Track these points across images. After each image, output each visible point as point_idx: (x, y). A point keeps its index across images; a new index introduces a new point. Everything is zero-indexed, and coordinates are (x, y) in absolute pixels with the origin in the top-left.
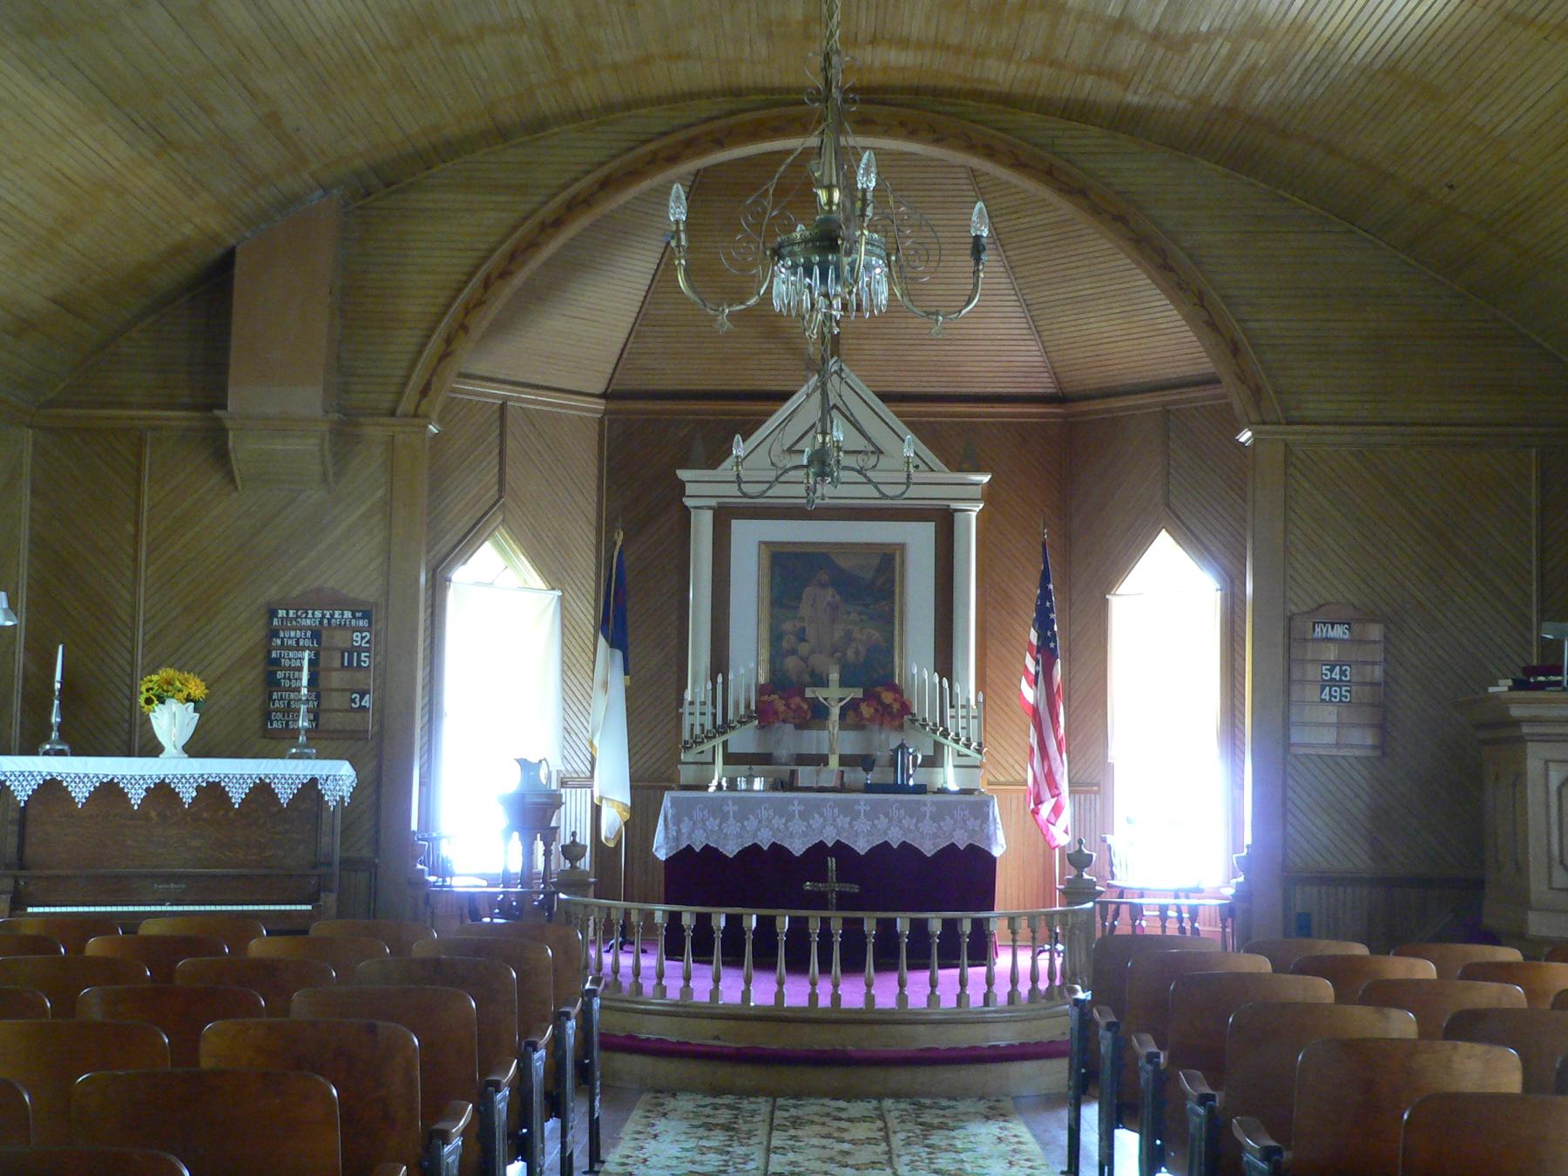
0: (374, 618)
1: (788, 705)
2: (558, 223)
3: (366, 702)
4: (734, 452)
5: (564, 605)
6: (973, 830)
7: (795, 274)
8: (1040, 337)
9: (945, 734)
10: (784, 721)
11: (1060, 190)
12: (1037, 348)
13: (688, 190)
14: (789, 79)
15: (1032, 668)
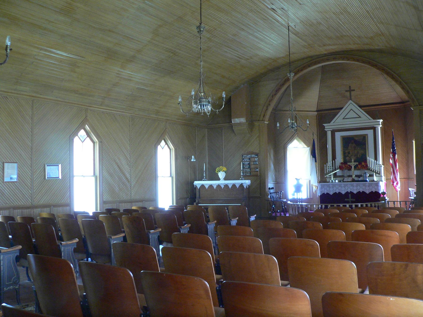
0: (258, 156)
1: (345, 166)
3: (258, 170)
10: (345, 169)
15: (391, 157)
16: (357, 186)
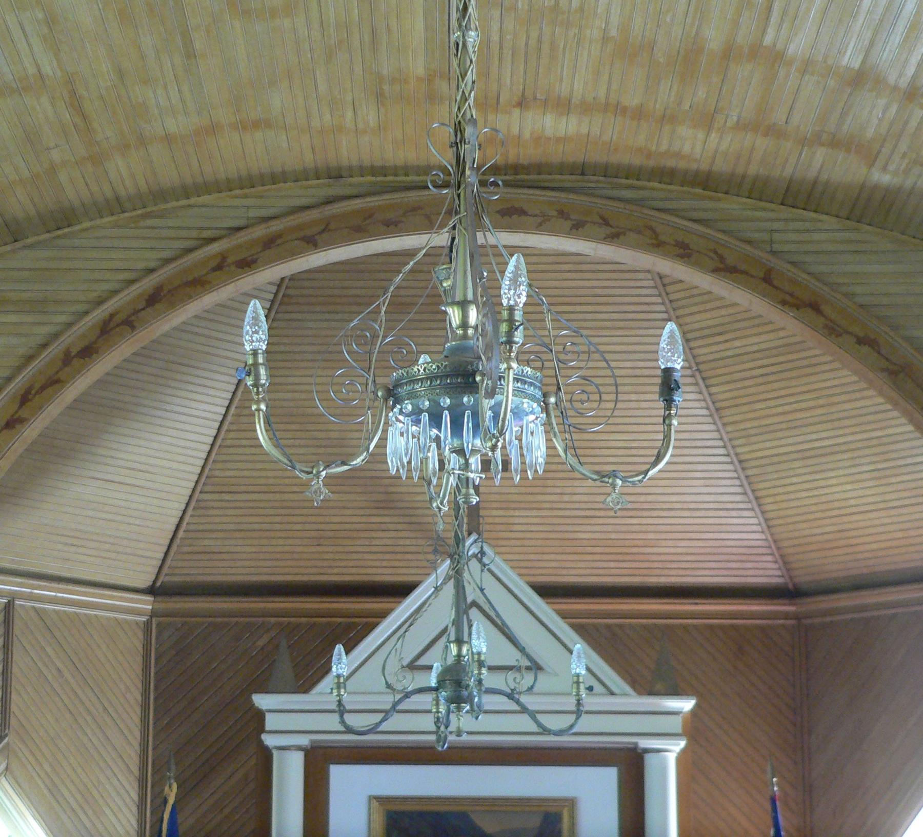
2: (88, 352)
4: (334, 669)
7: (417, 422)
8: (760, 505)
11: (784, 303)
12: (755, 521)
13: (268, 305)
14: (407, 155)
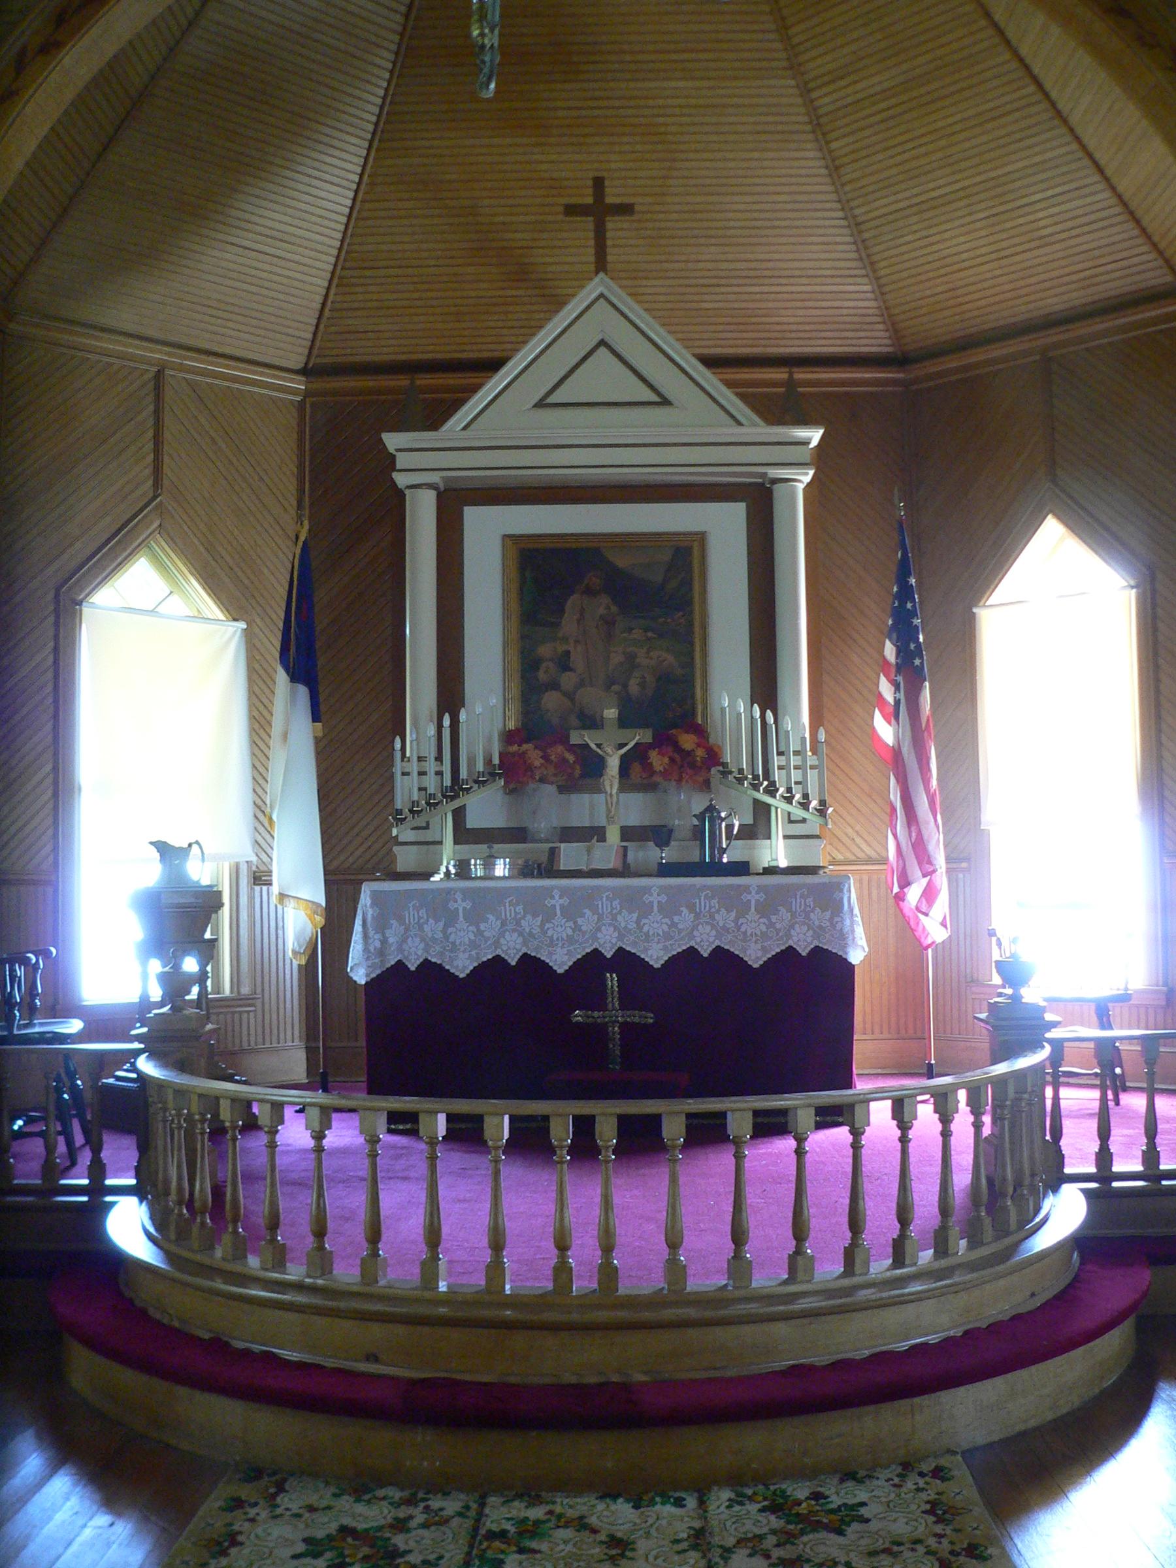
1: (546, 758)
5: (249, 637)
6: (820, 927)
9: (771, 791)
10: (542, 780)
12: (868, 288)
16: (669, 910)
